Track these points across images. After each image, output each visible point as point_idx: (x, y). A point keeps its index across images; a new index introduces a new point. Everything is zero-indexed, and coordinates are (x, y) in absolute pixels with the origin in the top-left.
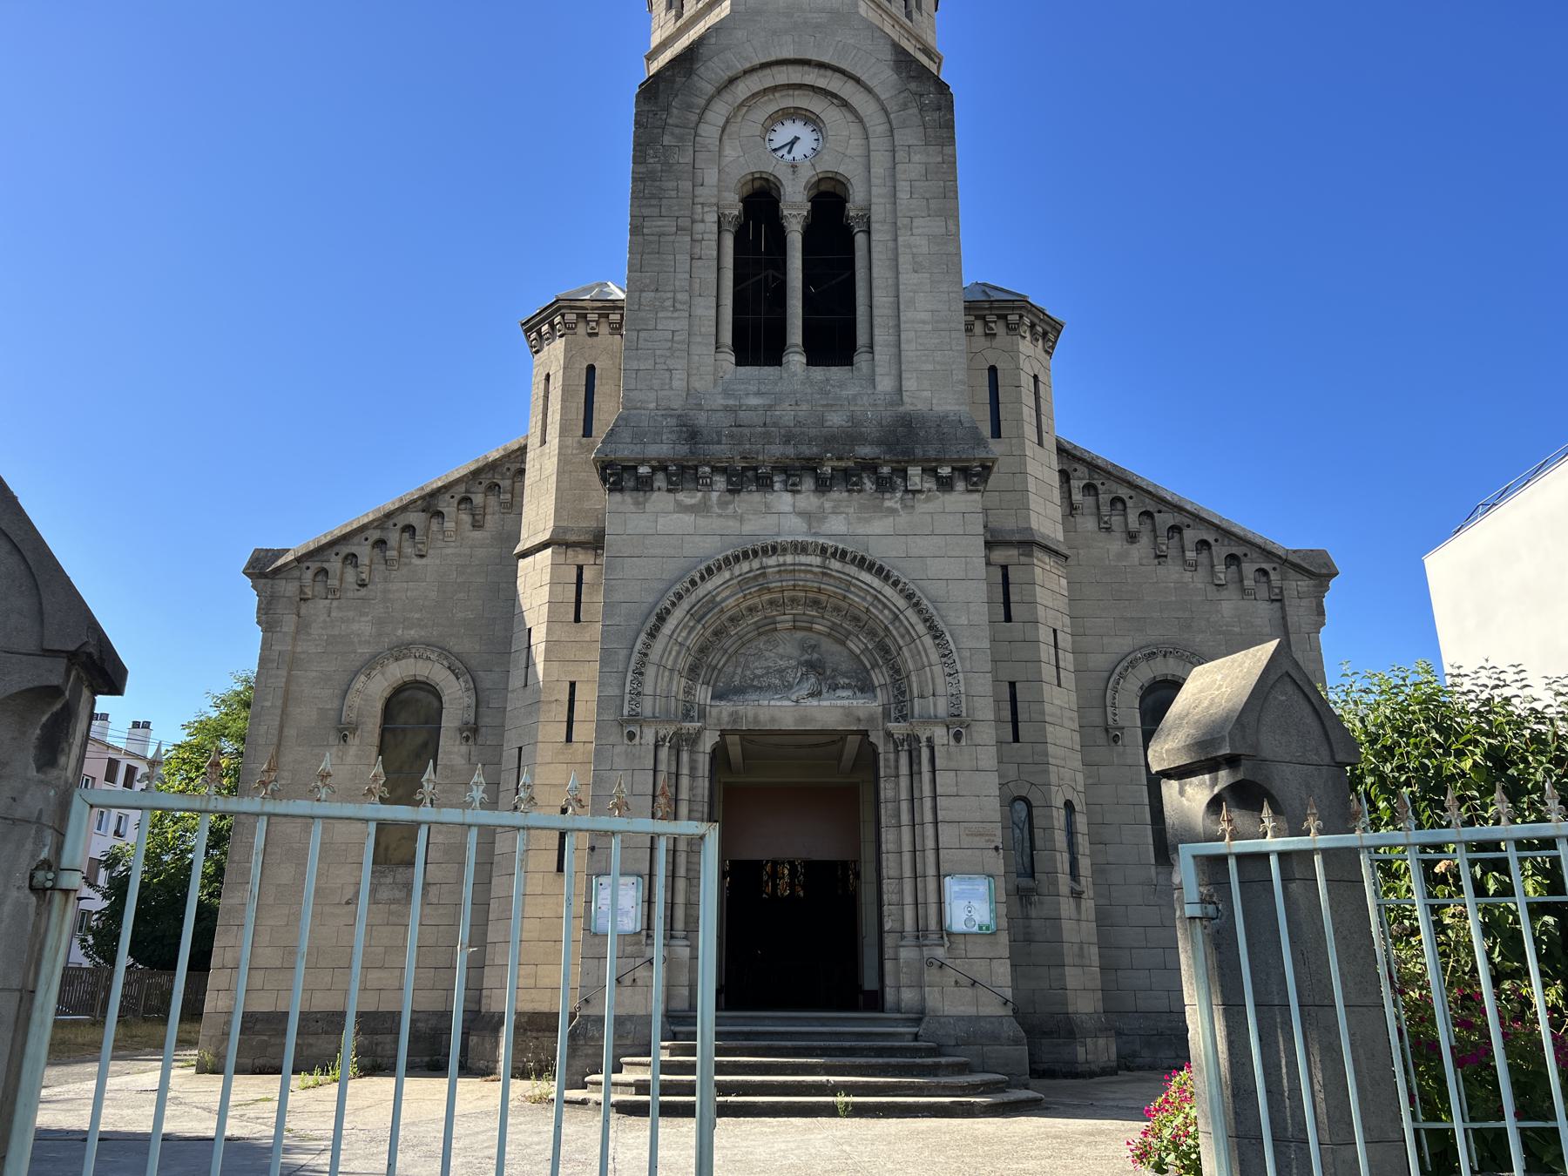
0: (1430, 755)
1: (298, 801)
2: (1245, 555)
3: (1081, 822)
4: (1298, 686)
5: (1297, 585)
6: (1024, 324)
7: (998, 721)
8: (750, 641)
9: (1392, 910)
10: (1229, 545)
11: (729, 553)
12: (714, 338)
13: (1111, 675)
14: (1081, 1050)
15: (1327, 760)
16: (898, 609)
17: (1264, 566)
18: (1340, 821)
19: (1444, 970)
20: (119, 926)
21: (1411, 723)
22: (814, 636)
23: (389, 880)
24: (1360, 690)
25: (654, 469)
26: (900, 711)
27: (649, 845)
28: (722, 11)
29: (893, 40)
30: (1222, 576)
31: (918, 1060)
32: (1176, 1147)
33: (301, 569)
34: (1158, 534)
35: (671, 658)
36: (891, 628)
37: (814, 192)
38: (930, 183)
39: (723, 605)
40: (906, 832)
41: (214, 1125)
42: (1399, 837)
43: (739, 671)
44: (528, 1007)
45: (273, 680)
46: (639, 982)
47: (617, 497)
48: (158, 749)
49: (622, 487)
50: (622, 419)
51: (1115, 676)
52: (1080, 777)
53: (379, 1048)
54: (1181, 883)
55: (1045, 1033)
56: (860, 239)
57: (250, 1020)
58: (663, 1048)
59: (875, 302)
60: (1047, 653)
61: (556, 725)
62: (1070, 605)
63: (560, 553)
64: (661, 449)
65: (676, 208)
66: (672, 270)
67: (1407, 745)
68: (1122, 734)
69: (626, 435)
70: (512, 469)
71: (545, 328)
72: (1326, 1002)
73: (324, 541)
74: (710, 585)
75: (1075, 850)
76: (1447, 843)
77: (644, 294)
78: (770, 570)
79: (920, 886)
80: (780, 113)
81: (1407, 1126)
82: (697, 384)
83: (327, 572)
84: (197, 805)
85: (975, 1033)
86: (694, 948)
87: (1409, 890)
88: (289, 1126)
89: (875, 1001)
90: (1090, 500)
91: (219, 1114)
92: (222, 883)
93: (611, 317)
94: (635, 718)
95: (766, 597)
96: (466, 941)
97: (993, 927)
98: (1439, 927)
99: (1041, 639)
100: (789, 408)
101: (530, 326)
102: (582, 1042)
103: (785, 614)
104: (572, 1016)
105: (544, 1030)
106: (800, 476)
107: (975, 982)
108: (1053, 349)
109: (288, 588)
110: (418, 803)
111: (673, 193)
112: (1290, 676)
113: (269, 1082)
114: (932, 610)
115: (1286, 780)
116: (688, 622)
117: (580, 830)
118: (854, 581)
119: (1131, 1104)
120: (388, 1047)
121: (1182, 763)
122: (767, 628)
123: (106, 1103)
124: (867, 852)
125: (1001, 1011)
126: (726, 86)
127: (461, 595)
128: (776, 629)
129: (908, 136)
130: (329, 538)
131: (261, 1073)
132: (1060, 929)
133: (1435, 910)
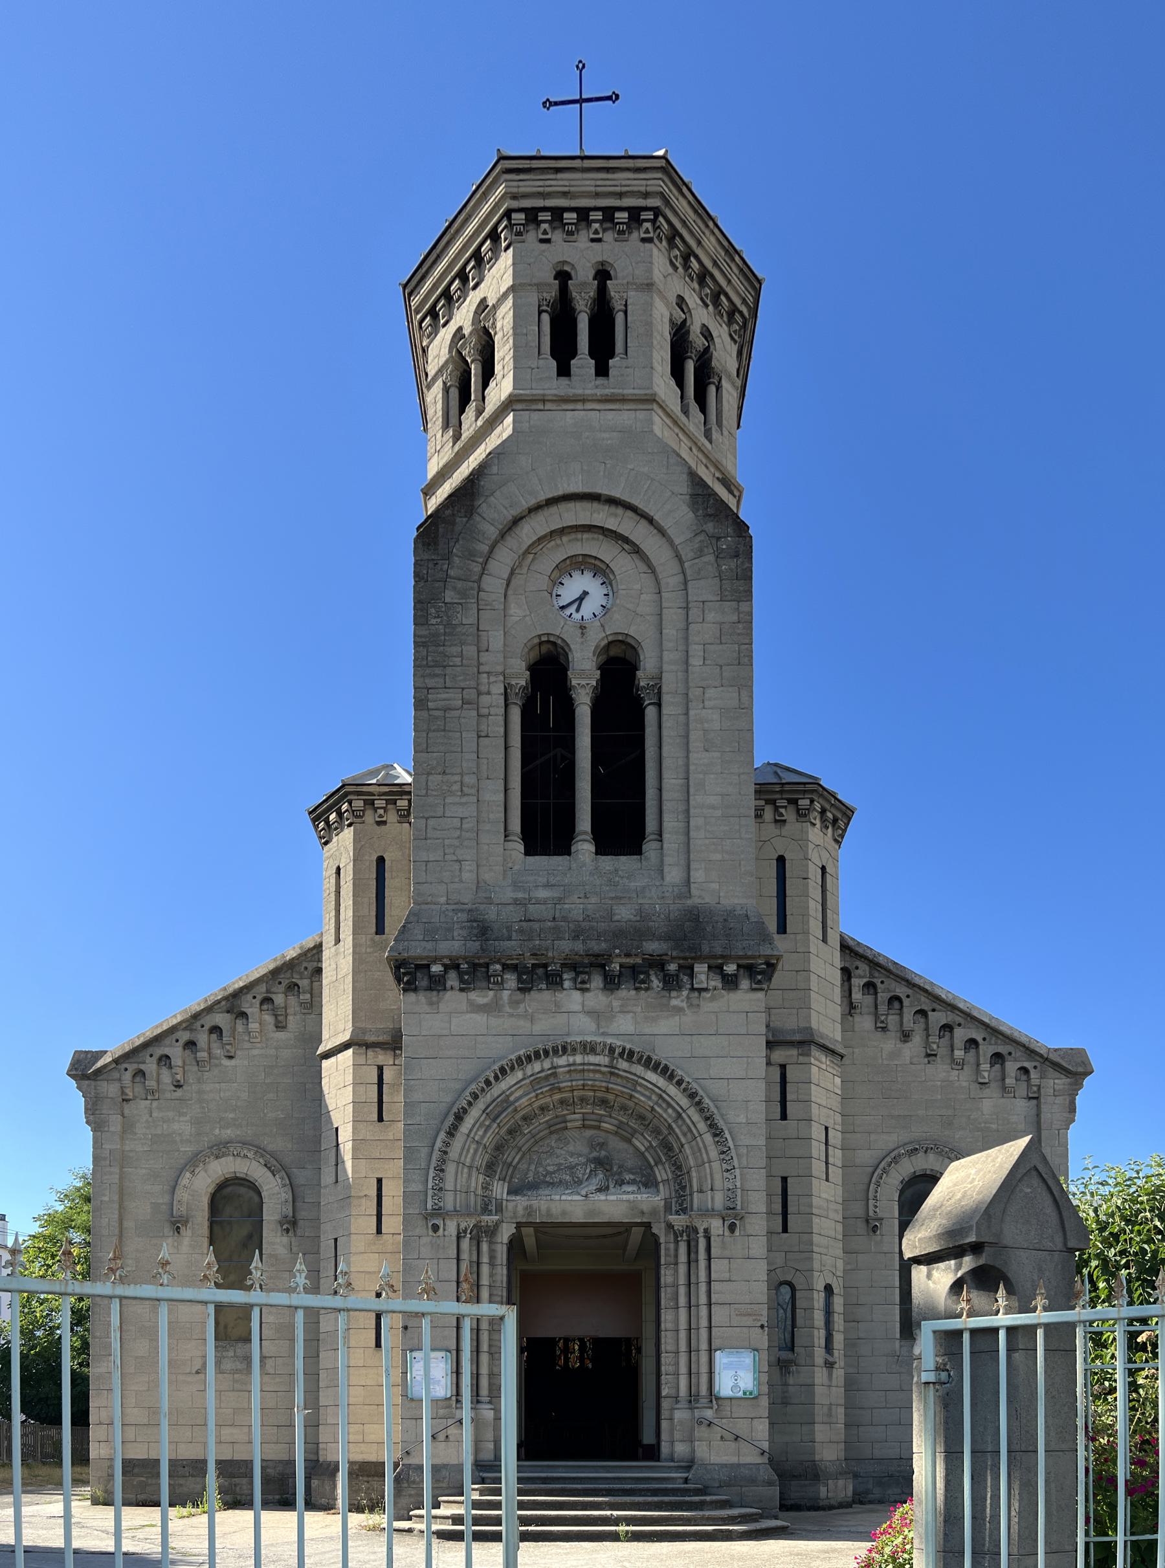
0: (1150, 1241)
1: (144, 1286)
2: (1010, 1054)
3: (838, 1303)
4: (1044, 1180)
5: (1055, 1083)
7: (770, 1213)
8: (542, 1139)
9: (1096, 1374)
10: (996, 1044)
11: (521, 1053)
12: (502, 826)
13: (875, 1170)
14: (823, 1490)
15: (1060, 1246)
16: (681, 1108)
17: (1026, 1064)
18: (1063, 1299)
19: (1131, 1421)
20: (9, 1388)
21: (1139, 1212)
22: (603, 1134)
23: (231, 1354)
24: (1098, 1183)
25: (447, 968)
26: (681, 1205)
27: (455, 1325)
28: (504, 430)
29: (690, 468)
30: (986, 1074)
31: (687, 1499)
32: (894, 1560)
33: (119, 1071)
35: (470, 1155)
36: (674, 1126)
37: (603, 658)
38: (724, 647)
39: (517, 1104)
40: (683, 1313)
41: (113, 1543)
42: (1112, 1312)
43: (533, 1167)
44: (359, 1458)
47: (412, 996)
48: (16, 1239)
50: (415, 915)
51: (879, 1171)
52: (840, 1264)
53: (238, 1489)
54: (920, 1354)
55: (794, 1476)
56: (650, 713)
57: (129, 1466)
58: (473, 1490)
59: (664, 785)
60: (818, 1149)
62: (842, 1103)
64: (454, 946)
66: (459, 750)
67: (1132, 1231)
68: (881, 1224)
69: (418, 932)
70: (310, 969)
71: (333, 817)
72: (1031, 1448)
73: (138, 1043)
74: (503, 1085)
76: (1151, 1317)
77: (431, 778)
78: (562, 1070)
80: (568, 562)
81: (1081, 1540)
82: (487, 876)
83: (144, 1074)
84: (57, 1288)
85: (736, 1477)
86: (497, 1411)
87: (1113, 1356)
88: (171, 1545)
89: (652, 1453)
90: (869, 999)
91: (115, 1535)
92: (89, 1355)
93: (399, 803)
94: (438, 1212)
95: (557, 1097)
96: (302, 1404)
97: (756, 1393)
98: (1133, 1387)
100: (578, 901)
101: (318, 815)
104: (396, 1465)
105: (373, 1476)
108: (842, 838)
109: (111, 1089)
110: (249, 1288)
111: (458, 661)
112: (1037, 1170)
113: (152, 1512)
114: (713, 1109)
115: (1021, 1265)
116: (484, 1121)
117: (394, 1312)
118: (640, 1080)
119: (861, 1529)
120: (245, 1487)
121: (932, 1250)
122: (558, 1127)
123: (24, 1525)
124: (648, 1331)
125: (759, 1460)
126: (510, 528)
127: (271, 1096)
128: (566, 1128)
129: (704, 589)
130: (142, 1040)
132: (813, 1394)
133: (1132, 1373)
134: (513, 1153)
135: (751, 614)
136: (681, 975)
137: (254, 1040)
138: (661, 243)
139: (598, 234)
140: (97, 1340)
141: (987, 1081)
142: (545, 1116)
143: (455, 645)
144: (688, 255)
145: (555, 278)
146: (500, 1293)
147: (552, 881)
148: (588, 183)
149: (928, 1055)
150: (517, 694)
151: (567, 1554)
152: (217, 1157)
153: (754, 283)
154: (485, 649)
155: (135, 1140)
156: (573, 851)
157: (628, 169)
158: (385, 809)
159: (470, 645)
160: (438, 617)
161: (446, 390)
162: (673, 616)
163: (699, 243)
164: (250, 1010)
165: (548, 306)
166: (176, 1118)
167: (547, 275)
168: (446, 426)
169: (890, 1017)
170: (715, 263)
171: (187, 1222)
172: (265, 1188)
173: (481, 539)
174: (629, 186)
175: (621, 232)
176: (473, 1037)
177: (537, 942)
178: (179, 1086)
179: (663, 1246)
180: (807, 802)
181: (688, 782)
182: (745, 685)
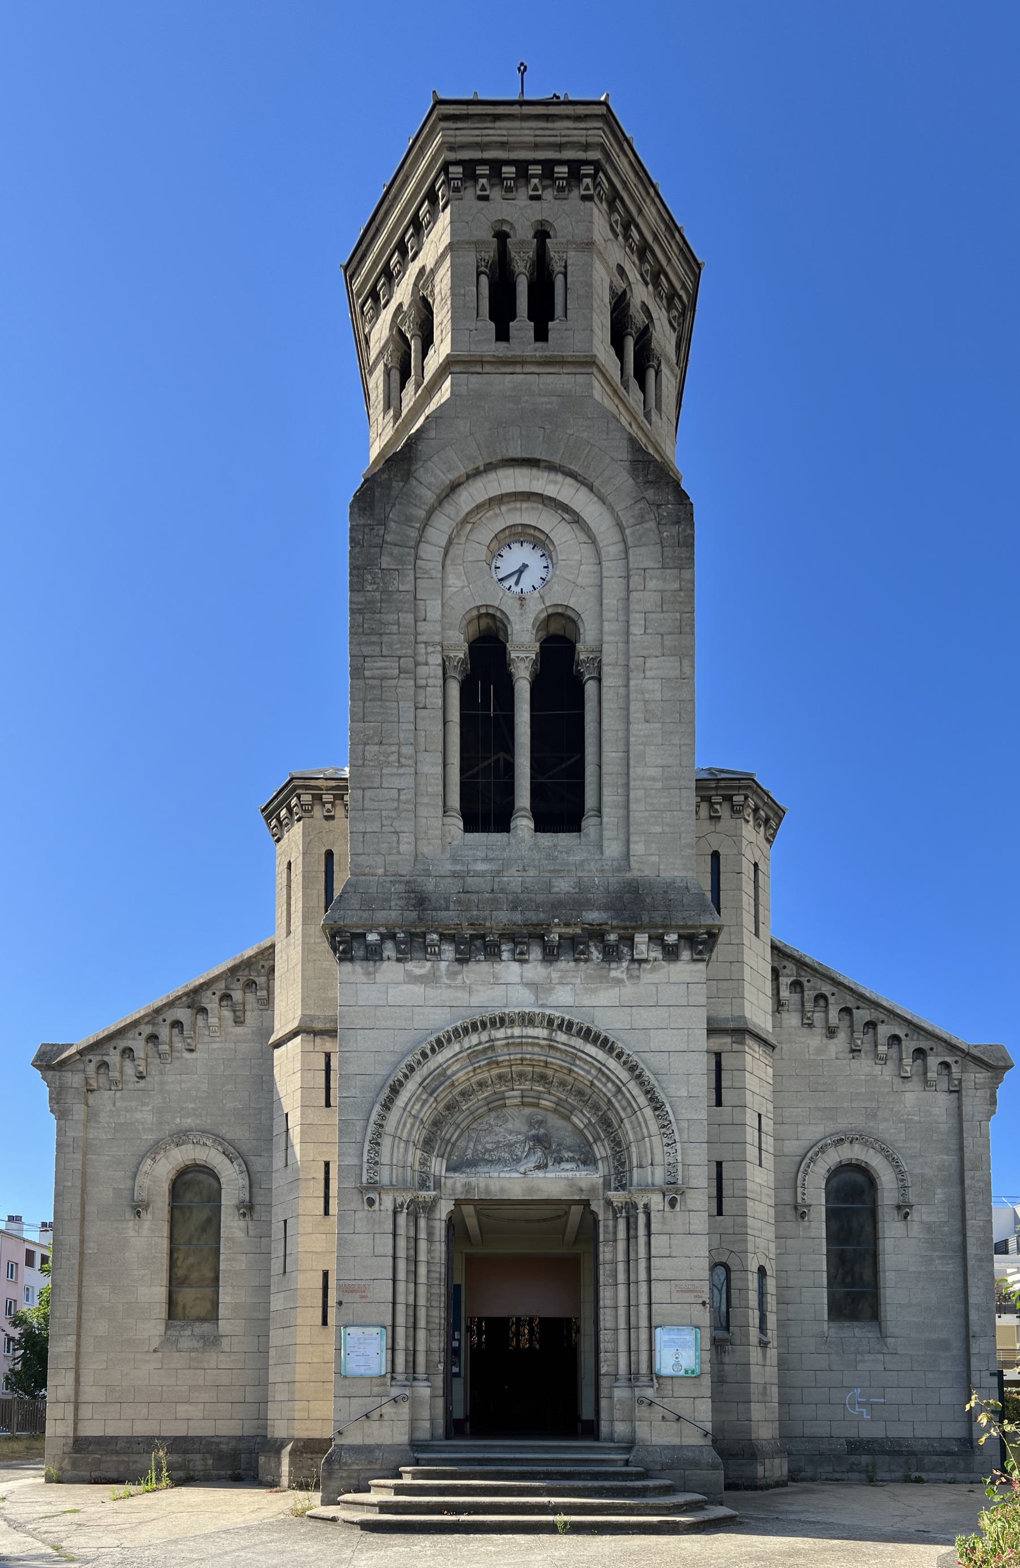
2: (932, 1049)
3: (771, 1284)
6: (749, 806)
10: (918, 1040)
11: (458, 1024)
14: (760, 1469)
16: (621, 1081)
17: (948, 1059)
22: (542, 1112)
23: (188, 1332)
25: (383, 937)
26: (620, 1181)
28: (442, 396)
30: (908, 1069)
33: (84, 1062)
34: (855, 1029)
35: (406, 1130)
36: (613, 1100)
37: (543, 634)
38: (666, 615)
39: (454, 1078)
45: (70, 1163)
46: (386, 1417)
47: (348, 967)
49: (352, 956)
50: (351, 885)
51: (806, 1160)
52: (772, 1246)
53: (191, 1464)
55: (731, 1455)
56: (590, 687)
59: (604, 759)
61: (315, 1200)
63: (309, 1041)
64: (391, 915)
65: (398, 646)
66: (396, 719)
70: (267, 967)
71: (283, 812)
74: (441, 1058)
75: (764, 1309)
77: (368, 748)
79: (633, 1336)
80: (507, 532)
82: (425, 849)
83: (108, 1065)
89: (591, 1430)
90: (796, 997)
97: (698, 1372)
99: (748, 1123)
101: (270, 812)
102: (337, 1467)
103: (513, 1090)
106: (528, 945)
107: (680, 1417)
108: (774, 838)
109: (74, 1079)
114: (653, 1081)
118: (580, 1054)
120: (198, 1463)
122: (497, 1103)
124: (587, 1311)
125: (701, 1442)
126: (447, 496)
127: (229, 1087)
128: (505, 1106)
129: (644, 557)
130: (106, 1033)
131: (96, 1483)
134: (452, 1130)
135: (693, 582)
136: (621, 946)
137: (215, 1034)
138: (601, 203)
139: (538, 190)
140: (56, 1320)
141: (909, 1075)
142: (483, 1093)
143: (391, 613)
144: (628, 223)
145: (494, 236)
146: (438, 1270)
147: (491, 855)
148: (527, 132)
149: (853, 1051)
150: (455, 667)
151: (497, 1553)
152: (177, 1145)
153: (694, 267)
154: (422, 617)
155: (99, 1128)
156: (512, 827)
157: (568, 117)
158: (333, 803)
159: (406, 612)
160: (375, 583)
161: (387, 372)
162: (613, 586)
163: (640, 211)
164: (210, 1005)
165: (486, 267)
166: (139, 1108)
167: (485, 234)
168: (387, 406)
169: (816, 1015)
170: (656, 237)
171: (147, 1206)
172: (223, 1174)
173: (418, 504)
174: (569, 136)
175: (561, 189)
176: (411, 1008)
177: (475, 913)
178: (142, 1078)
179: (601, 1224)
180: (742, 798)
181: (628, 756)
182: (685, 654)
